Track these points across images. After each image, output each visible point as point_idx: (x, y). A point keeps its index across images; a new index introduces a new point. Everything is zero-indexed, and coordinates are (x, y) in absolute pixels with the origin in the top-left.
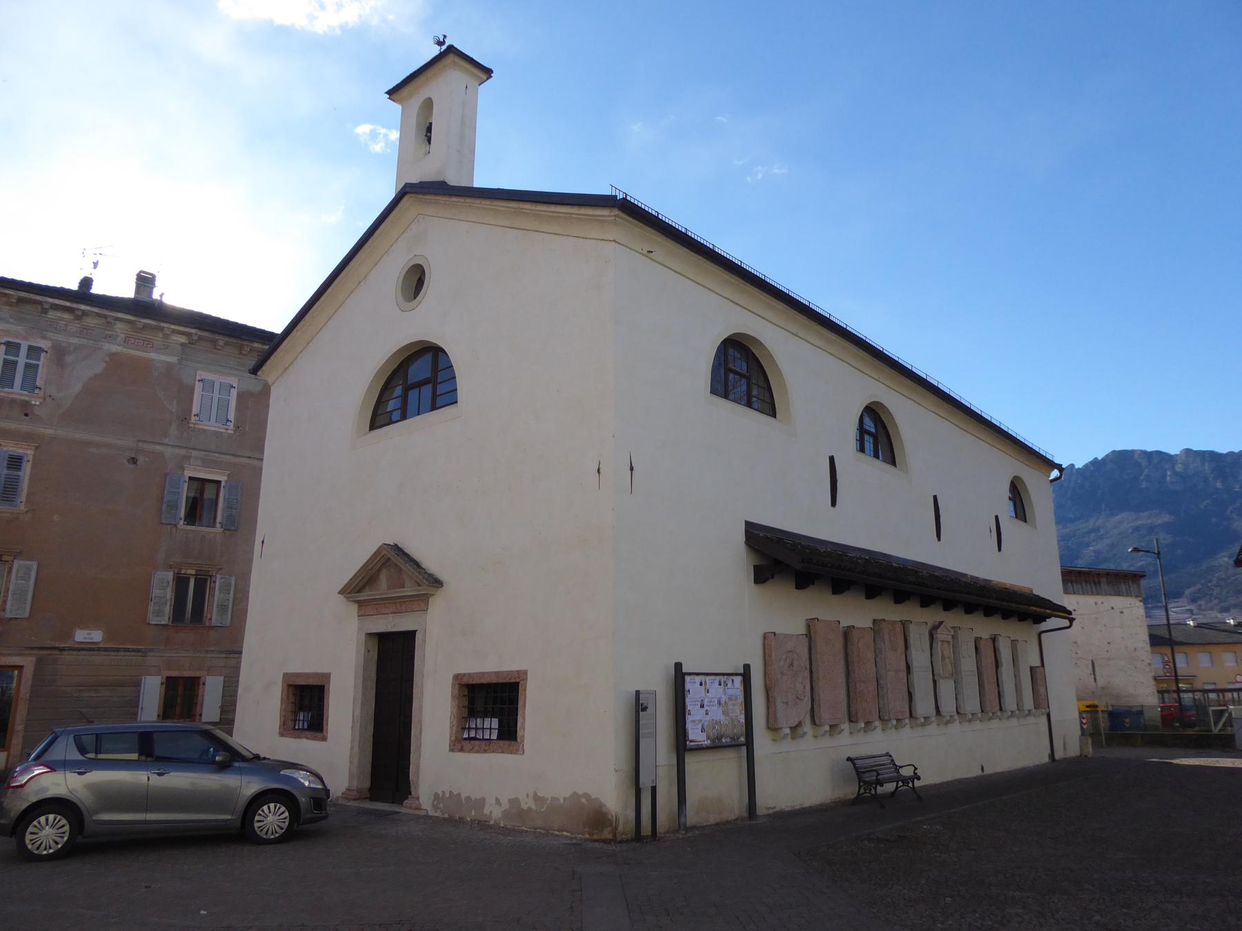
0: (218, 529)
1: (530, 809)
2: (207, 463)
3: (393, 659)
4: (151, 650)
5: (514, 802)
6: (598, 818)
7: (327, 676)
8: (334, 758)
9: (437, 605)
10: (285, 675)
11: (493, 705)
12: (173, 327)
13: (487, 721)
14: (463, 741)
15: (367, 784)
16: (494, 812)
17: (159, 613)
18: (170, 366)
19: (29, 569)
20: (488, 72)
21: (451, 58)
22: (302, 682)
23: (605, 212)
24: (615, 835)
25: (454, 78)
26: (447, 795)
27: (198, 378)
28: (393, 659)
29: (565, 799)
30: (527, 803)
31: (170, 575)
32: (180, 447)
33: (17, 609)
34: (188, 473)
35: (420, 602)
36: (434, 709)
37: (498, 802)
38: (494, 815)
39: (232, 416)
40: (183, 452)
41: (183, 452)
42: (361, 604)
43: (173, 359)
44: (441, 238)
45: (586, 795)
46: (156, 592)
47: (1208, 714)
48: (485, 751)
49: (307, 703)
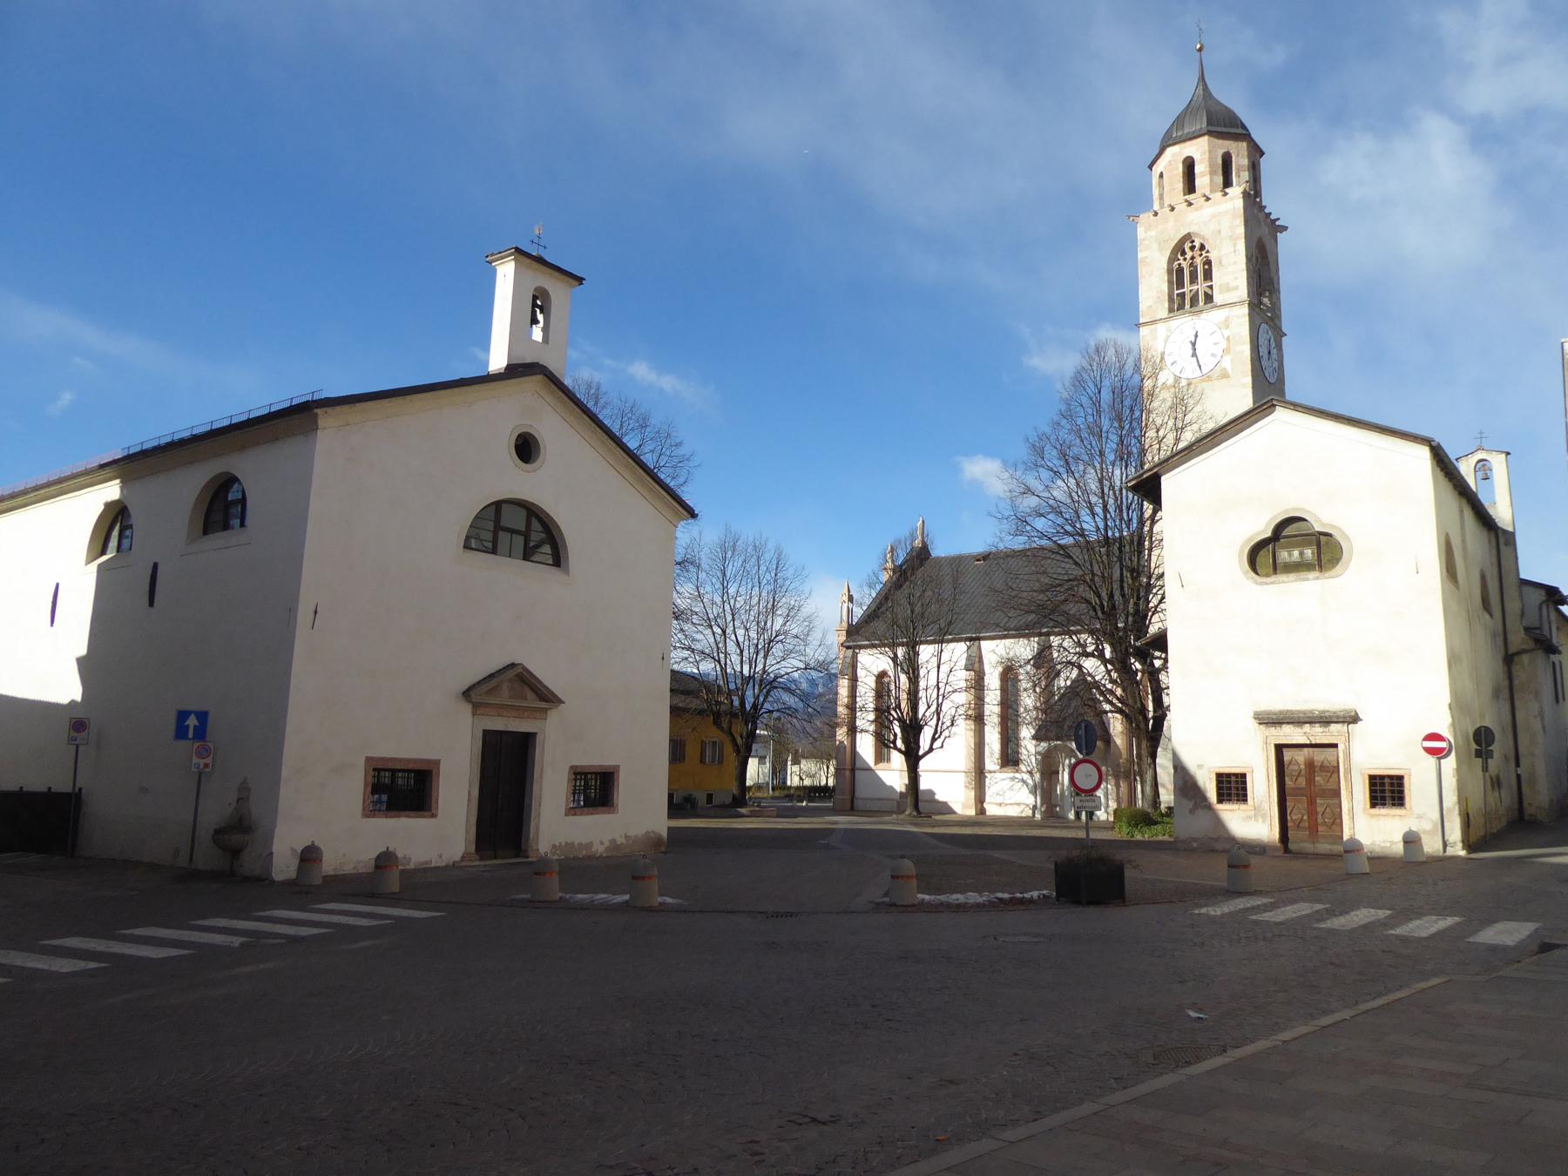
7: (437, 763)
9: (554, 716)
11: (596, 789)
15: (473, 848)
16: (599, 849)
21: (533, 383)
30: (620, 840)
49: (402, 789)
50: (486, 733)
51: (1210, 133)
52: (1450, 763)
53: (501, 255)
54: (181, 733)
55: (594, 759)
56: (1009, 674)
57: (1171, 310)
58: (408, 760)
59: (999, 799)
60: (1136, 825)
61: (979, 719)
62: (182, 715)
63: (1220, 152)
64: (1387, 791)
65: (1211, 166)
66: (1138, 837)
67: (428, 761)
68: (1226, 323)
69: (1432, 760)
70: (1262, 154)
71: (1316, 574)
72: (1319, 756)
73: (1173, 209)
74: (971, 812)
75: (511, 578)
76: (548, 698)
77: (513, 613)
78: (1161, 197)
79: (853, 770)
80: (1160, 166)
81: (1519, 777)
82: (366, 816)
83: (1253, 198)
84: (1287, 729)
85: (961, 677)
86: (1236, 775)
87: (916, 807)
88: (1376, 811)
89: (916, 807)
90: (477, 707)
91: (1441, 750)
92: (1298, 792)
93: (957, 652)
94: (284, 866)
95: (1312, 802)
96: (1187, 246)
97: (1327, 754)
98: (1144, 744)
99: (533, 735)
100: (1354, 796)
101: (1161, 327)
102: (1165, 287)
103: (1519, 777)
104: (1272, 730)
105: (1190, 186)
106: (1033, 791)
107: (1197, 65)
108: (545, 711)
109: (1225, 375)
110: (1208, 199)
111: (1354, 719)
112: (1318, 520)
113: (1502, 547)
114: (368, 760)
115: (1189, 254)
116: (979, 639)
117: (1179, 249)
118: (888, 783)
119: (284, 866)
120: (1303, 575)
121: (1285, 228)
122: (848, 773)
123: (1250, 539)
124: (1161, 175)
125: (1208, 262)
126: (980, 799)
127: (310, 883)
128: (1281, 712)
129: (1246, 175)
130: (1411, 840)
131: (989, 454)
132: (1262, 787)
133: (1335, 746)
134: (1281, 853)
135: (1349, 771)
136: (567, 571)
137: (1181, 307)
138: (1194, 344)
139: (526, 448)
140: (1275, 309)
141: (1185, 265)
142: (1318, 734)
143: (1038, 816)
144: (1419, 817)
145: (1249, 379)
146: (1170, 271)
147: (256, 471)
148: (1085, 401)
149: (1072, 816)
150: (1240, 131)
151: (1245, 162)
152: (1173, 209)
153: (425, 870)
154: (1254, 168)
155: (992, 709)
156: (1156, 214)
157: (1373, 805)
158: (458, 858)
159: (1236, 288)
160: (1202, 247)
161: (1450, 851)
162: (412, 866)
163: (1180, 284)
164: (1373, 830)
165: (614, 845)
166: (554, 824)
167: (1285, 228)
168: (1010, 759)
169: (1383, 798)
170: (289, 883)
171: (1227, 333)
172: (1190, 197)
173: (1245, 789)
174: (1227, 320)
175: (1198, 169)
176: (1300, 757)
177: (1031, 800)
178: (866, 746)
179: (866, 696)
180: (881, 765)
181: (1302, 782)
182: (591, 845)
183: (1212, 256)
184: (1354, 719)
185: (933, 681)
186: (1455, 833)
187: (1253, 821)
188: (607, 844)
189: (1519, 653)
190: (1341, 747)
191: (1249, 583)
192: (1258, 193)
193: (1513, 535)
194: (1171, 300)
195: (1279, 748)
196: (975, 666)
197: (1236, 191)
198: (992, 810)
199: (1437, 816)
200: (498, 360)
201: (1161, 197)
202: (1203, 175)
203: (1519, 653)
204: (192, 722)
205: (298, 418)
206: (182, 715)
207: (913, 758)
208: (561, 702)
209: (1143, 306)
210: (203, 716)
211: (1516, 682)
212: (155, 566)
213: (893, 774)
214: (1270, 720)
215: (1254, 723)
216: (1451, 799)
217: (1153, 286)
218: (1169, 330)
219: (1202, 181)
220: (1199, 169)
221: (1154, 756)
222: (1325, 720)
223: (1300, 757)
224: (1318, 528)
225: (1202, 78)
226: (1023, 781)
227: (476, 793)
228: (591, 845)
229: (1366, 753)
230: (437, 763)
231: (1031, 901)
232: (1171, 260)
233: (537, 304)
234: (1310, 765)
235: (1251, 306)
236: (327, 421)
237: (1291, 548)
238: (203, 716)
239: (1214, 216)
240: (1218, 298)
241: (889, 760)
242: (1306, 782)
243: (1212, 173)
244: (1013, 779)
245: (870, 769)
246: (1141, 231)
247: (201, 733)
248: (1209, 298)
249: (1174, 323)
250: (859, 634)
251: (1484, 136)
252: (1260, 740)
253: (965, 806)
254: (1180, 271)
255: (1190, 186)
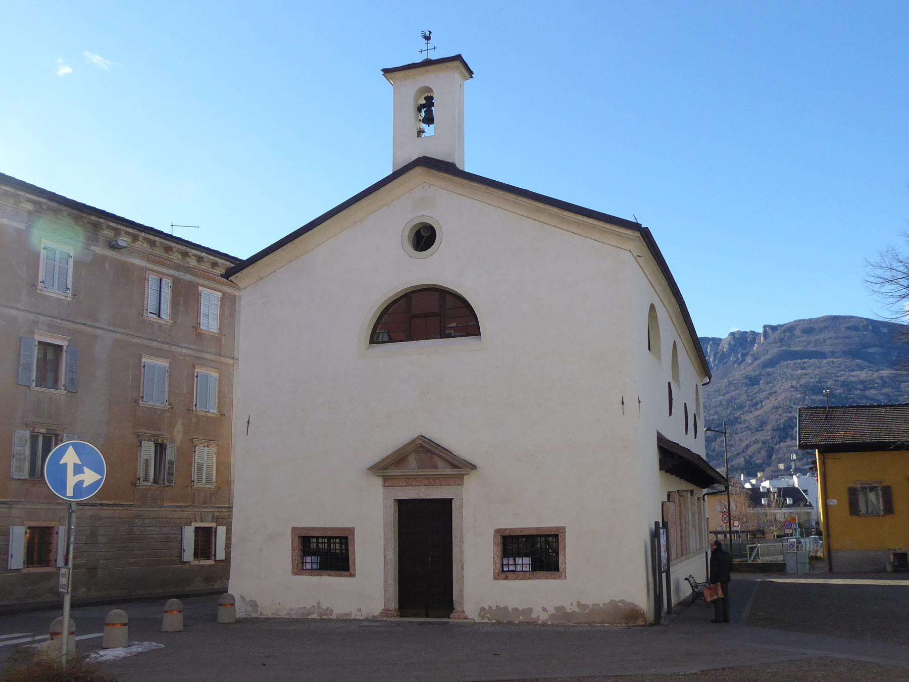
0: (62, 391)
1: (574, 612)
2: (52, 329)
4: (16, 503)
6: (633, 614)
7: (352, 531)
8: (369, 587)
9: (471, 483)
11: (535, 551)
12: (28, 195)
13: (519, 560)
15: (394, 605)
17: (20, 469)
18: (19, 232)
20: (471, 73)
21: (457, 63)
22: (507, 533)
23: (629, 232)
24: (646, 622)
25: (455, 74)
26: (494, 608)
27: (43, 246)
29: (604, 604)
31: (27, 433)
32: (30, 312)
34: (38, 337)
35: (458, 479)
37: (544, 609)
38: (541, 618)
39: (70, 285)
40: (32, 317)
41: (32, 317)
42: (386, 479)
43: (22, 226)
44: (443, 205)
45: (622, 601)
46: (17, 449)
47: (28, 575)
48: (529, 578)
49: (327, 552)
50: (401, 503)
62: (889, 509)
67: (344, 529)
76: (460, 468)
99: (448, 503)
108: (461, 477)
114: (294, 529)
139: (424, 238)
153: (346, 621)
158: (377, 613)
162: (334, 617)
166: (480, 583)
182: (530, 610)
188: (552, 611)
208: (473, 467)
228: (530, 610)
230: (352, 531)
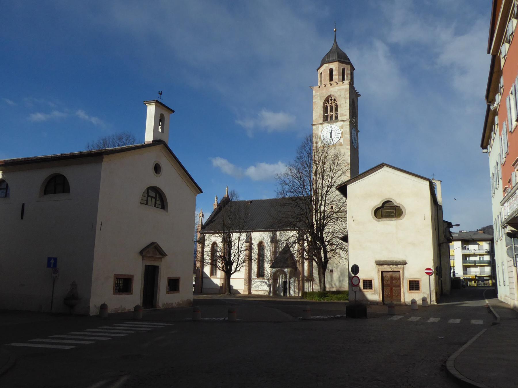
3: (151, 274)
5: (179, 302)
7: (132, 276)
9: (164, 260)
10: (115, 275)
14: (168, 292)
16: (175, 305)
19: (331, 71)
21: (159, 147)
28: (151, 274)
30: (181, 302)
33: (515, 21)
36: (163, 285)
49: (123, 285)
51: (339, 61)
52: (433, 277)
53: (150, 102)
54: (49, 265)
55: (174, 275)
56: (261, 245)
57: (323, 121)
58: (125, 275)
59: (256, 289)
60: (321, 297)
61: (250, 260)
62: (49, 259)
63: (342, 68)
64: (414, 285)
65: (339, 72)
66: (322, 301)
68: (342, 127)
69: (428, 276)
70: (354, 69)
71: (395, 219)
72: (394, 275)
73: (325, 86)
74: (247, 293)
75: (153, 213)
76: (163, 254)
77: (152, 226)
78: (321, 81)
79: (202, 278)
80: (321, 70)
81: (441, 281)
82: (114, 294)
83: (351, 84)
84: (385, 266)
85: (245, 246)
86: (369, 280)
87: (230, 292)
88: (411, 291)
89: (230, 292)
90: (144, 257)
91: (431, 273)
92: (388, 286)
93: (244, 235)
94: (93, 311)
95: (392, 289)
96: (330, 99)
97: (397, 274)
98: (321, 270)
100: (405, 287)
101: (320, 126)
102: (322, 112)
103: (441, 281)
104: (381, 267)
105: (331, 79)
106: (269, 286)
107: (334, 38)
109: (341, 144)
110: (337, 84)
111: (405, 263)
112: (396, 202)
113: (439, 211)
115: (330, 102)
116: (251, 232)
117: (327, 100)
118: (215, 283)
119: (93, 311)
120: (391, 219)
121: (360, 95)
122: (200, 279)
123: (375, 207)
124: (321, 73)
125: (336, 105)
126: (249, 288)
127: (105, 317)
128: (383, 261)
129: (349, 76)
130: (424, 300)
131: (223, 156)
132: (377, 284)
133: (399, 272)
134: (382, 304)
135: (403, 279)
136: (167, 211)
137: (327, 120)
138: (331, 133)
139: (157, 169)
140: (356, 122)
141: (328, 105)
142: (394, 268)
143: (271, 294)
144: (424, 293)
145: (349, 147)
146: (323, 107)
147: (72, 174)
148: (305, 154)
149: (282, 295)
150: (348, 61)
151: (349, 72)
152: (325, 86)
154: (352, 74)
155: (255, 256)
156: (319, 87)
157: (410, 290)
159: (346, 115)
160: (335, 100)
161: (432, 303)
162: (126, 311)
163: (327, 112)
164: (407, 296)
165: (179, 304)
166: (164, 298)
167: (360, 95)
168: (261, 274)
169: (413, 287)
170: (96, 316)
171: (342, 130)
172: (331, 82)
173: (372, 285)
174: (342, 126)
175: (334, 73)
176: (389, 275)
177: (268, 289)
178: (207, 270)
179: (208, 249)
180: (213, 276)
181: (389, 283)
183: (338, 103)
184: (405, 263)
185: (236, 247)
186: (434, 298)
187: (374, 295)
189: (443, 243)
190: (401, 272)
191: (375, 221)
192: (353, 84)
193: (442, 206)
194: (324, 117)
195: (382, 272)
196: (249, 240)
197: (347, 82)
198: (254, 292)
199: (429, 293)
200: (149, 138)
201: (321, 81)
202: (336, 75)
203: (443, 243)
204: (52, 261)
205: (95, 157)
206: (49, 259)
207: (228, 274)
209: (314, 118)
210: (55, 259)
211: (441, 252)
212: (23, 205)
213: (218, 280)
214: (379, 263)
215: (374, 265)
216: (433, 287)
217: (318, 112)
218: (323, 127)
219: (335, 77)
220: (335, 73)
221: (324, 274)
222: (396, 263)
223: (389, 275)
224: (396, 204)
225: (335, 41)
226: (266, 283)
227: (143, 286)
229: (410, 273)
230: (132, 276)
231: (338, 318)
232: (324, 103)
233: (160, 119)
234: (391, 277)
235: (351, 122)
236: (106, 159)
237: (388, 210)
238: (55, 259)
239: (339, 90)
240: (339, 118)
241: (216, 274)
242: (391, 282)
243: (339, 75)
244: (262, 281)
245: (208, 278)
246: (314, 92)
247: (55, 265)
248: (336, 118)
249: (324, 125)
250: (208, 227)
251: (395, 51)
252: (376, 269)
253: (244, 291)
254: (327, 107)
255: (331, 79)
